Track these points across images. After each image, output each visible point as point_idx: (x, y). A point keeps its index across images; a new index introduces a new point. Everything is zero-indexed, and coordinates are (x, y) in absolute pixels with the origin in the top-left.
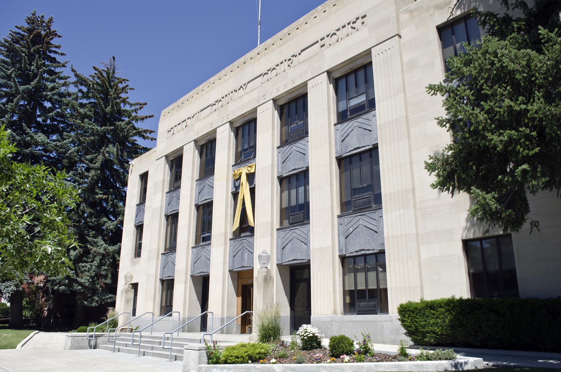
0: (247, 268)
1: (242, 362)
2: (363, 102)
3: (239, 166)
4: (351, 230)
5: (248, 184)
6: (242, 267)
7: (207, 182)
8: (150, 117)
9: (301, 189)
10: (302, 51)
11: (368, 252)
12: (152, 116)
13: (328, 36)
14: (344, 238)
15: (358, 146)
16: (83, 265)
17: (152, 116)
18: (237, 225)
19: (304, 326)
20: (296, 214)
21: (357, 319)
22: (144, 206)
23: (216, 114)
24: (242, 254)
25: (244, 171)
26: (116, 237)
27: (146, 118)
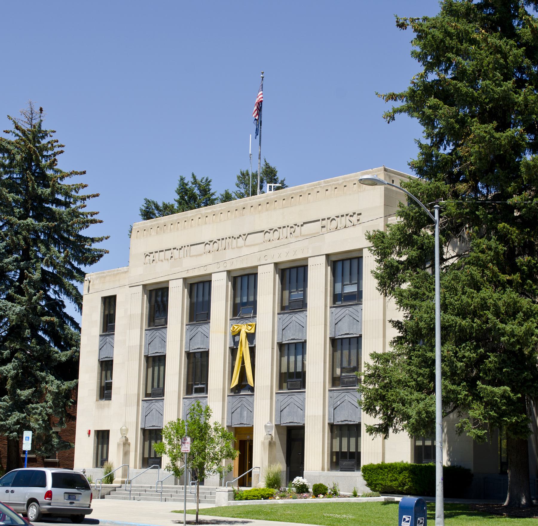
0: (246, 426)
1: (257, 499)
2: (355, 292)
3: (238, 321)
4: (339, 403)
5: (247, 342)
6: (241, 424)
7: (199, 329)
8: (94, 196)
9: (299, 358)
10: (304, 223)
11: (350, 423)
12: (97, 195)
13: (328, 219)
14: (332, 409)
15: (348, 332)
16: (33, 406)
17: (97, 195)
18: (235, 382)
19: (298, 478)
20: (292, 380)
21: (339, 475)
22: (113, 339)
23: (210, 256)
24: (241, 411)
25: (244, 329)
26: (70, 370)
27: (89, 197)
